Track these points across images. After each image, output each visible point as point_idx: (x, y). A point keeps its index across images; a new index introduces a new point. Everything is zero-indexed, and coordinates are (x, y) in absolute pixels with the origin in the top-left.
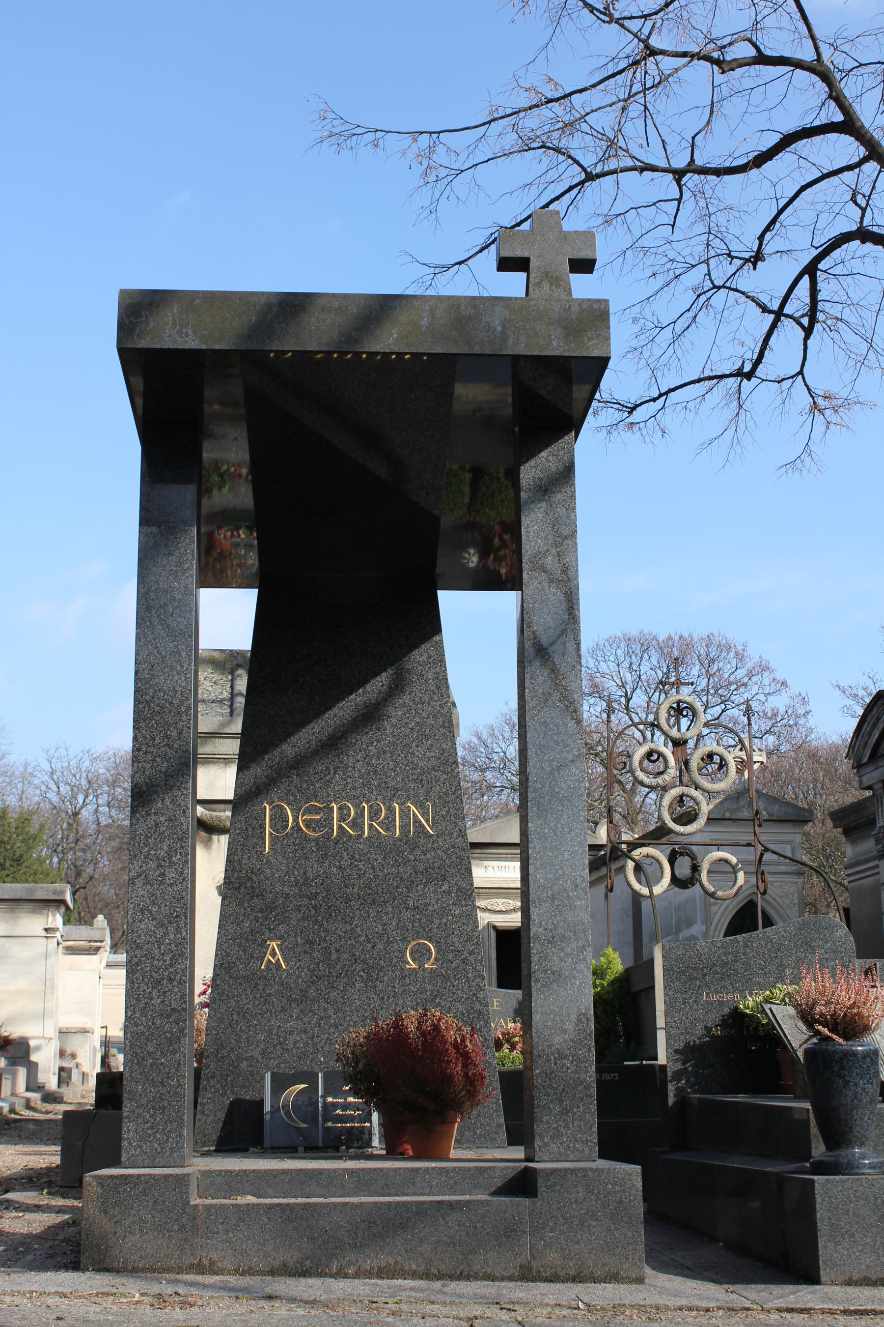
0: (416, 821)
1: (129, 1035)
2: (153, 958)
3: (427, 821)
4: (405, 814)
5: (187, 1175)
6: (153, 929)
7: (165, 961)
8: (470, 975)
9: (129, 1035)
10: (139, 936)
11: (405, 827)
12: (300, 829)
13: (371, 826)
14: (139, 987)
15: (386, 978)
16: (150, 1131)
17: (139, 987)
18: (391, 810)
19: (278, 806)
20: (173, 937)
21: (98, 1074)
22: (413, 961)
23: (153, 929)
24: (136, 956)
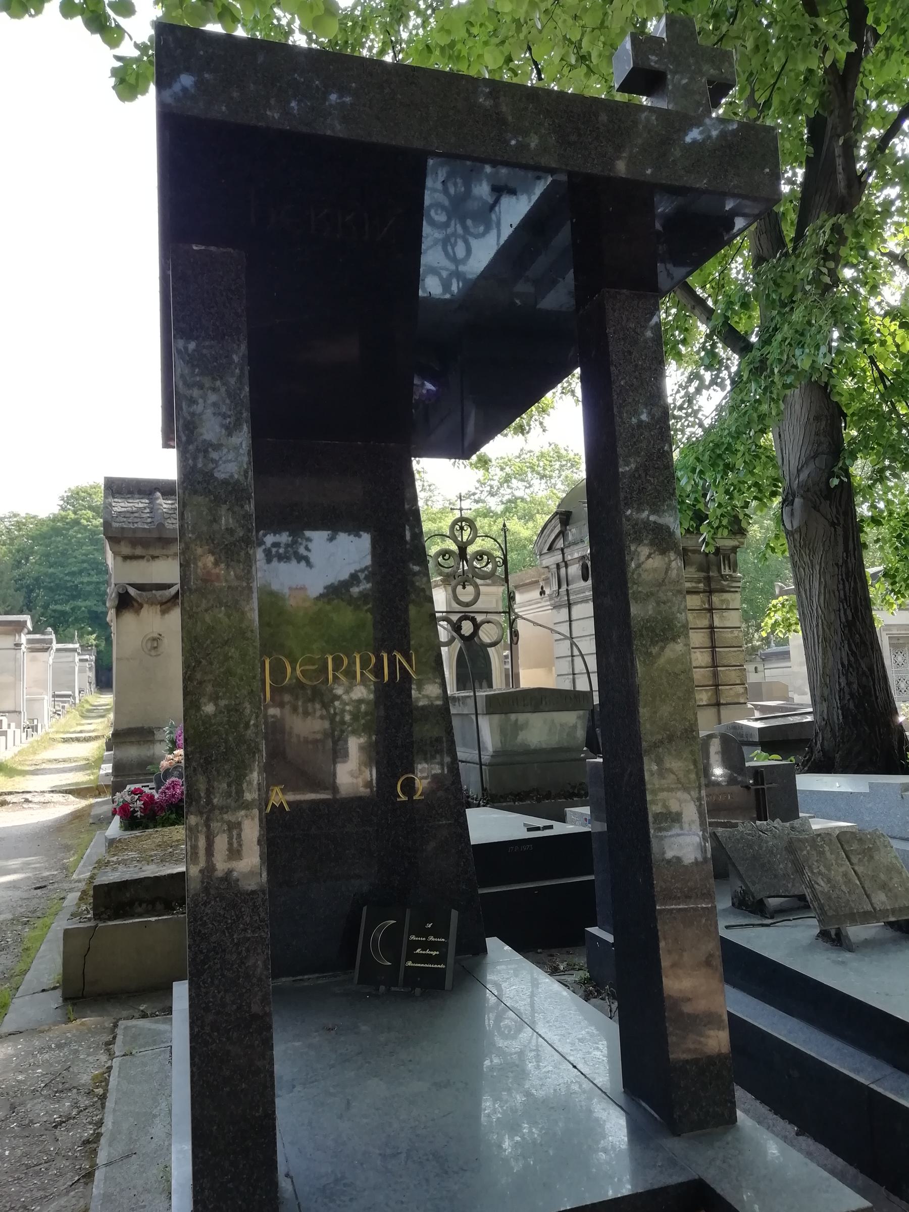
0: (402, 667)
1: (196, 1060)
2: (224, 951)
3: (411, 666)
4: (392, 661)
5: (169, 1010)
6: (222, 912)
7: (240, 953)
8: (451, 804)
9: (196, 1060)
10: (204, 924)
11: (392, 672)
12: (291, 663)
13: (362, 674)
14: (206, 993)
15: (380, 812)
16: (230, 1185)
17: (206, 993)
18: (380, 660)
19: (276, 659)
20: (248, 920)
21: (67, 933)
22: (404, 793)
23: (222, 912)
24: (201, 952)
